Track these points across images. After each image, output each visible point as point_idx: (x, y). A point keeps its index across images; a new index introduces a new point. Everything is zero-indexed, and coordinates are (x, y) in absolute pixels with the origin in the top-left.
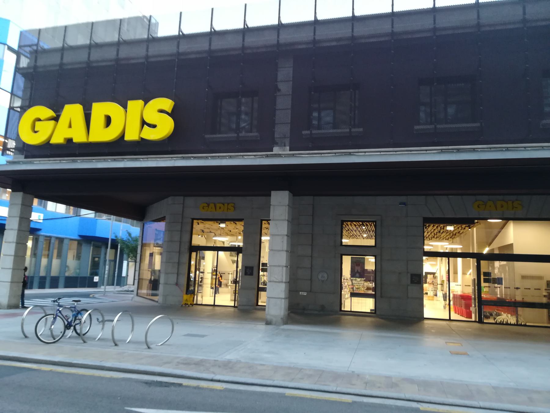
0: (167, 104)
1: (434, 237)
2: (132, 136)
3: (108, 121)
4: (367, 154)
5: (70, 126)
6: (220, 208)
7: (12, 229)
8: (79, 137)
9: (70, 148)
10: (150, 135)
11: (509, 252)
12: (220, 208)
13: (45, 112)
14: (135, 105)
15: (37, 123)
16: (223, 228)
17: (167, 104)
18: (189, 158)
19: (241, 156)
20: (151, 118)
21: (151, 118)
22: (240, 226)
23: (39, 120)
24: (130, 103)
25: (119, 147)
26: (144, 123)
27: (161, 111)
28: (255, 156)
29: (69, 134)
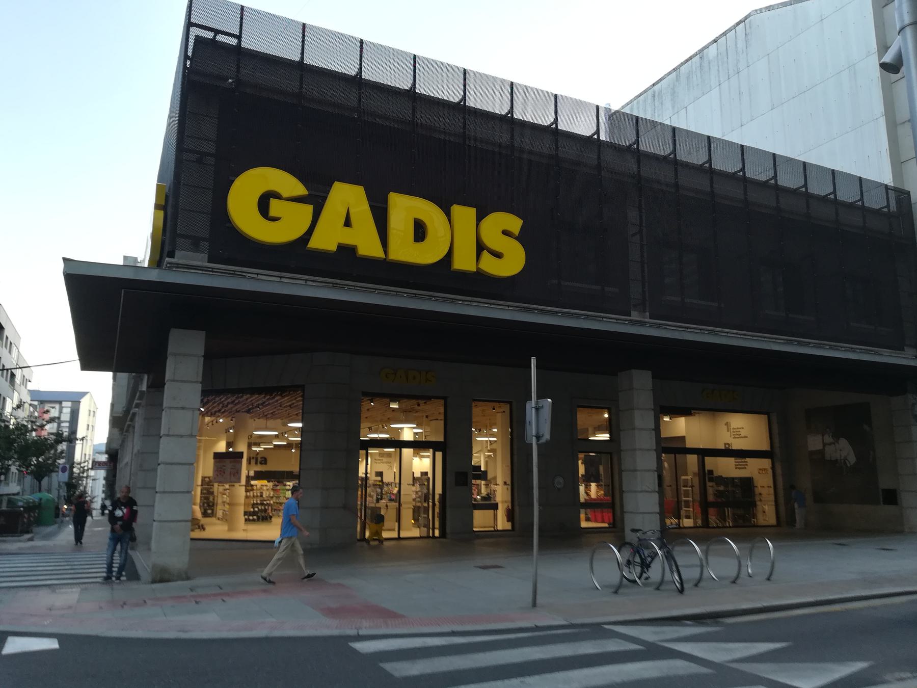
0: (515, 224)
1: (220, 411)
2: (464, 262)
3: (420, 231)
4: (260, 277)
5: (348, 223)
6: (414, 378)
7: (183, 408)
8: (368, 244)
9: (345, 263)
10: (490, 265)
11: (679, 445)
12: (414, 378)
13: (287, 184)
14: (464, 214)
15: (273, 202)
16: (394, 410)
17: (515, 224)
18: (532, 310)
19: (600, 317)
20: (492, 242)
21: (492, 242)
22: (437, 407)
23: (277, 196)
24: (456, 209)
25: (441, 276)
26: (481, 247)
27: (506, 233)
28: (617, 319)
29: (348, 237)
